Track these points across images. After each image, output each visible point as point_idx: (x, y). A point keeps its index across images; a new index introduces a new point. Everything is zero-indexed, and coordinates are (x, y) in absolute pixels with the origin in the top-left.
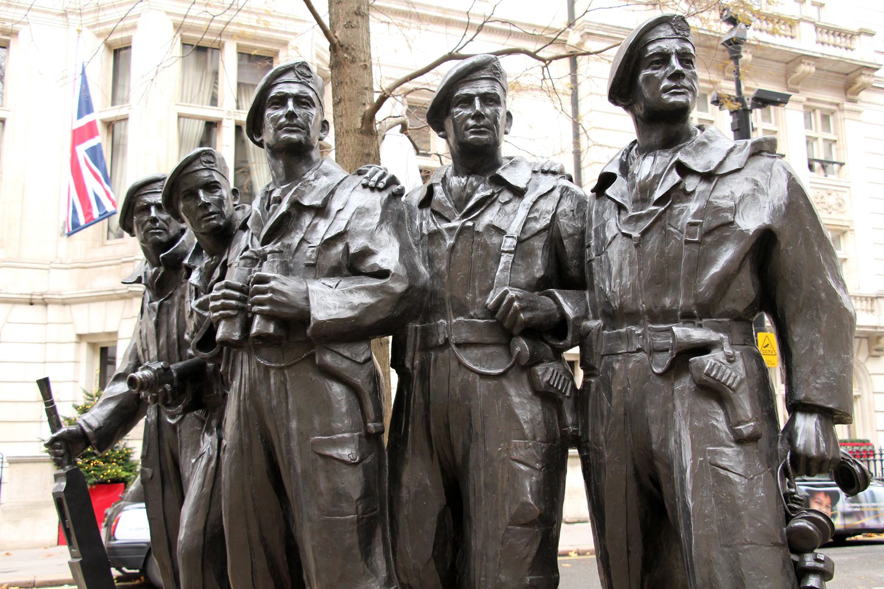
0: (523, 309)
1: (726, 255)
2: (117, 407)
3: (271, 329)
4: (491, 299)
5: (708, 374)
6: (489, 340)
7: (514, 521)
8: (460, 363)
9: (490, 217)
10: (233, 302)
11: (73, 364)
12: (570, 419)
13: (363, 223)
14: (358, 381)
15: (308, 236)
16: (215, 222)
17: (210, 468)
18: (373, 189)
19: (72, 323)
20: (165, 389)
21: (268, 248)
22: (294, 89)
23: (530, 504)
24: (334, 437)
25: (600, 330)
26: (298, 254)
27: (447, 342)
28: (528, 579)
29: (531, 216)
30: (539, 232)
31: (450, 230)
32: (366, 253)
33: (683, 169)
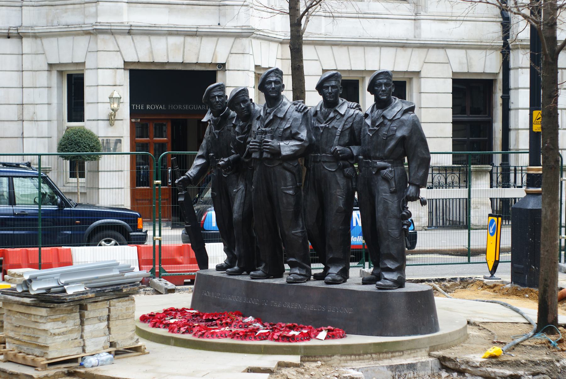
0: (340, 154)
1: (393, 143)
2: (200, 169)
3: (269, 156)
4: (332, 150)
5: (384, 175)
6: (332, 161)
7: (337, 212)
8: (324, 167)
9: (334, 123)
10: (257, 147)
11: (47, 89)
12: (354, 184)
13: (296, 123)
14: (295, 171)
15: (279, 127)
16: (246, 113)
17: (243, 195)
18: (299, 112)
19: (44, 54)
20: (229, 168)
21: (267, 129)
22: (274, 79)
23: (341, 207)
24: (288, 187)
25: (362, 159)
26: (276, 132)
27: (320, 161)
28: (341, 227)
29: (346, 123)
30: (348, 129)
31: (322, 127)
32: (298, 133)
33: (384, 117)
